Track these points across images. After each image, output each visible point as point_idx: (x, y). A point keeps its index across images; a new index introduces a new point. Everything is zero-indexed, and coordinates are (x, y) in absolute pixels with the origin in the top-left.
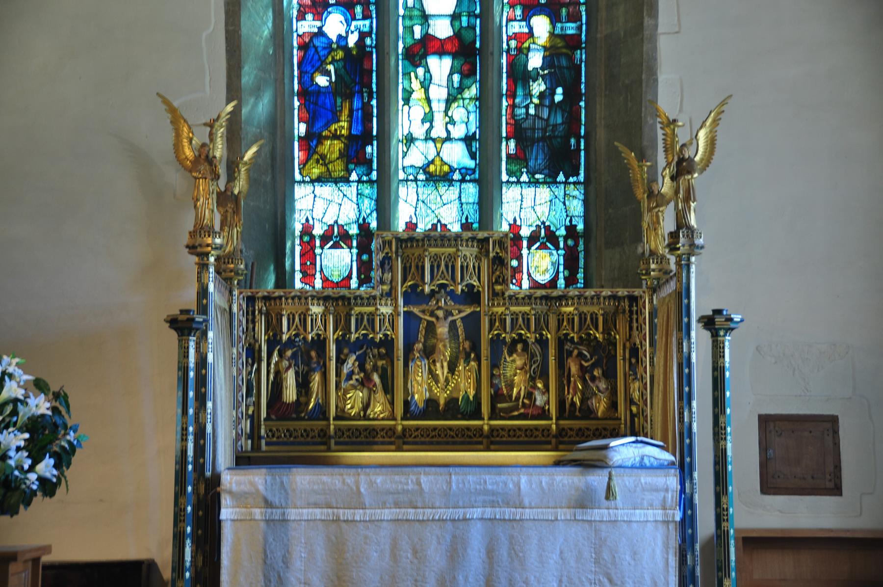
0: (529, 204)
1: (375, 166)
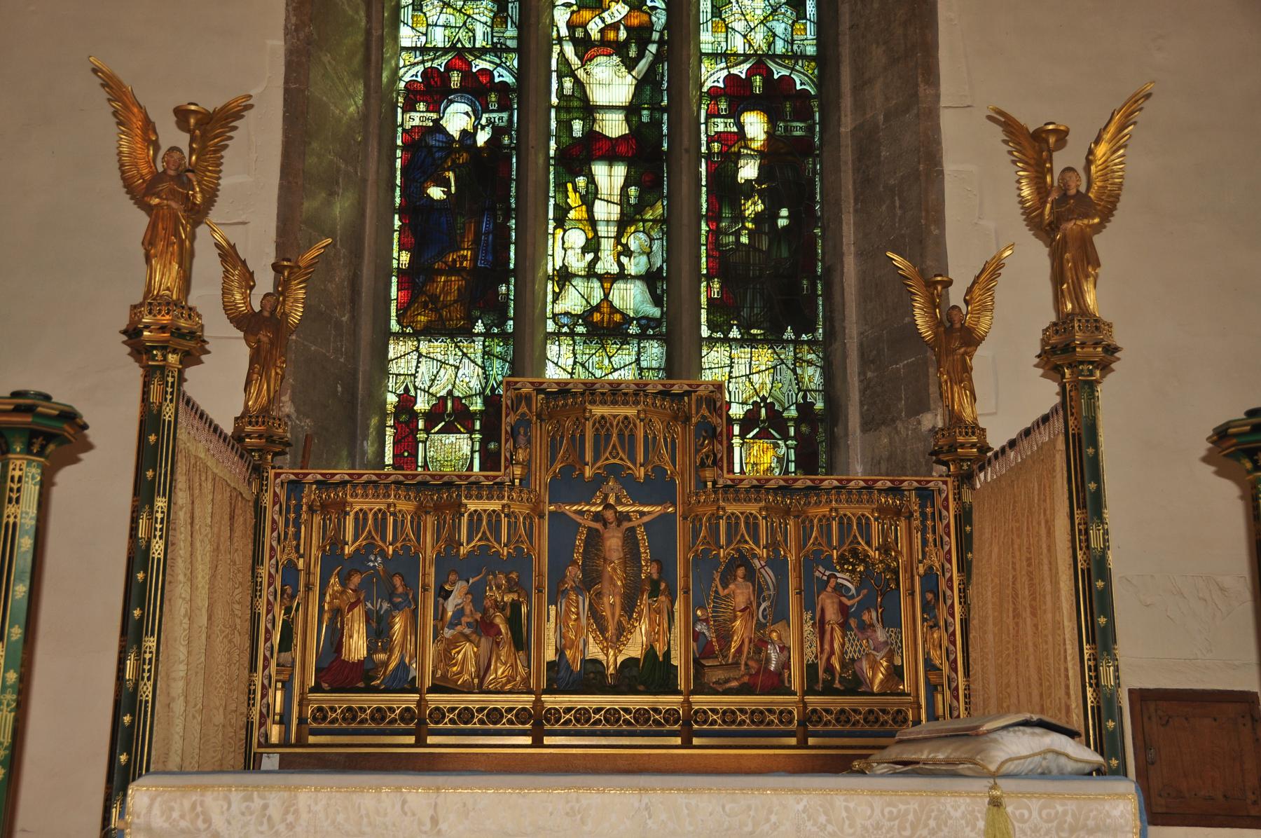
0: (741, 371)
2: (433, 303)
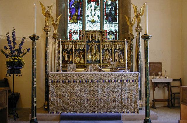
0: (108, 27)
1: (82, 20)
2: (73, 20)
